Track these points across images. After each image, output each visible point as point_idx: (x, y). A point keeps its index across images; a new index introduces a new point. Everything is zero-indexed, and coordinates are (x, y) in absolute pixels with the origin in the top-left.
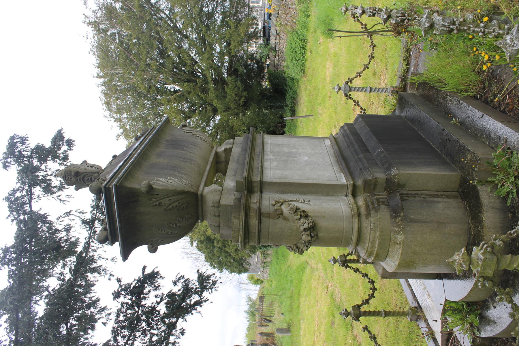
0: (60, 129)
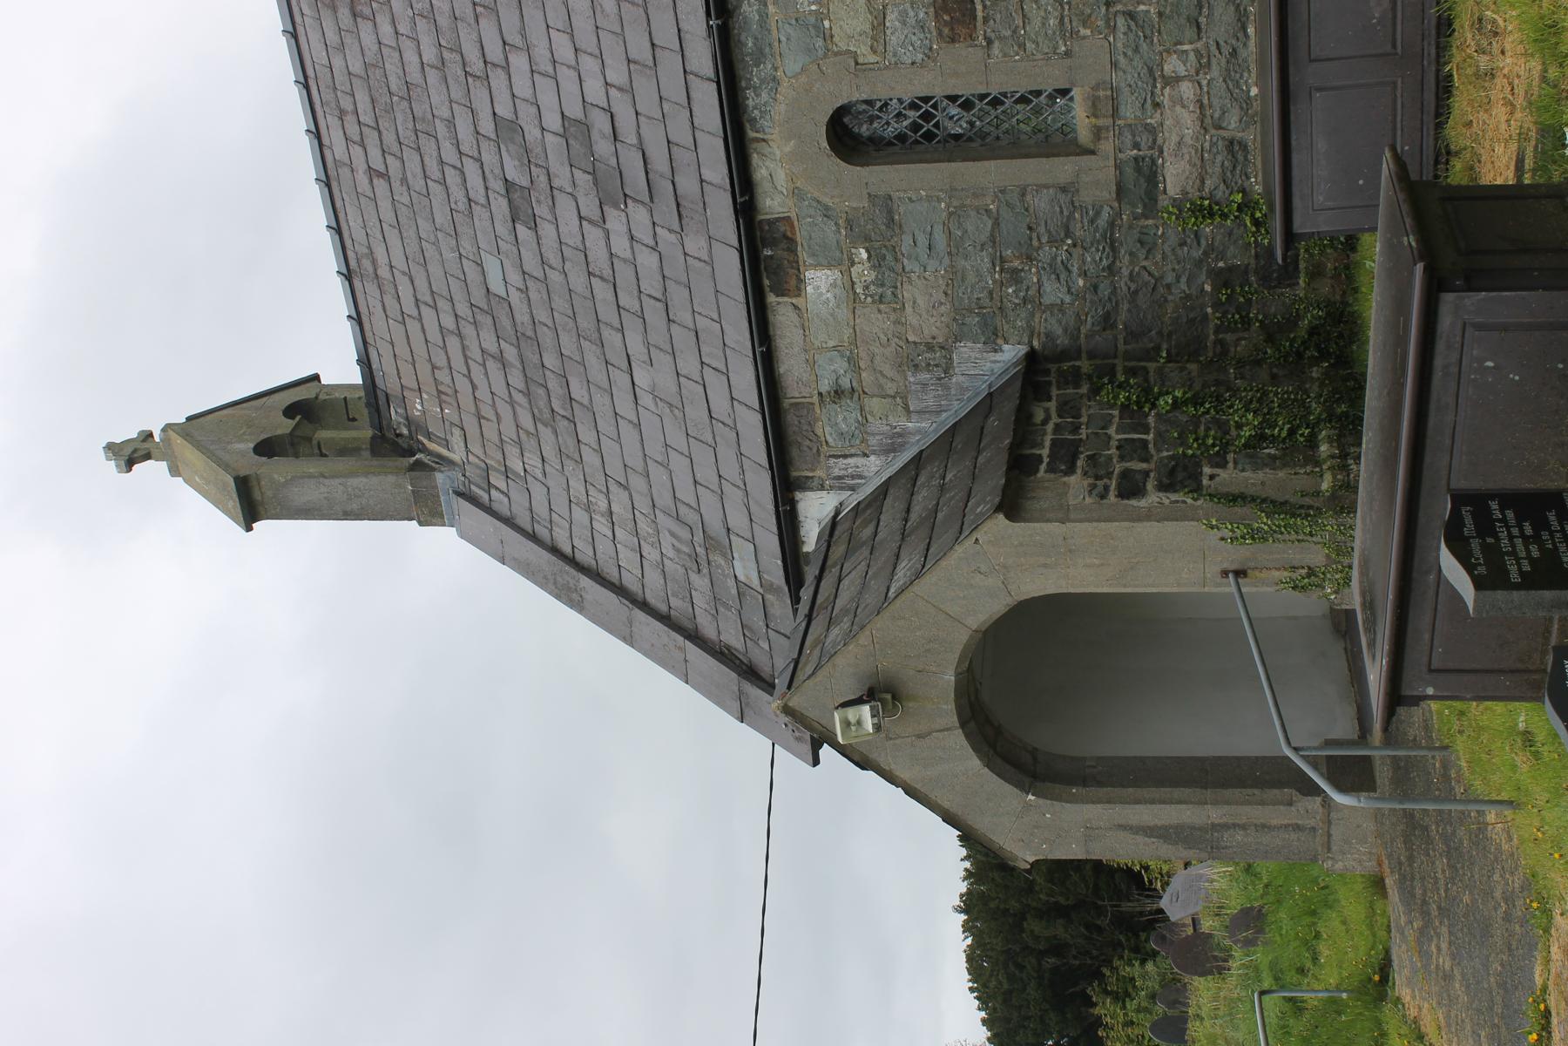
0: (182, 515)
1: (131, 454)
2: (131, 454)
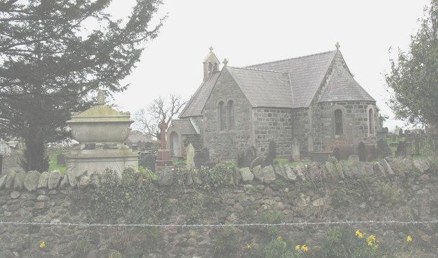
0: (205, 55)
1: (211, 49)
2: (211, 49)
